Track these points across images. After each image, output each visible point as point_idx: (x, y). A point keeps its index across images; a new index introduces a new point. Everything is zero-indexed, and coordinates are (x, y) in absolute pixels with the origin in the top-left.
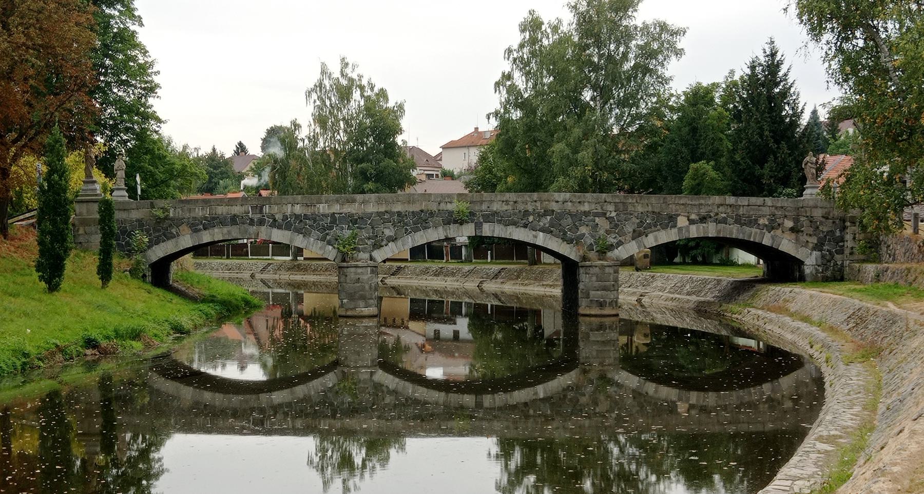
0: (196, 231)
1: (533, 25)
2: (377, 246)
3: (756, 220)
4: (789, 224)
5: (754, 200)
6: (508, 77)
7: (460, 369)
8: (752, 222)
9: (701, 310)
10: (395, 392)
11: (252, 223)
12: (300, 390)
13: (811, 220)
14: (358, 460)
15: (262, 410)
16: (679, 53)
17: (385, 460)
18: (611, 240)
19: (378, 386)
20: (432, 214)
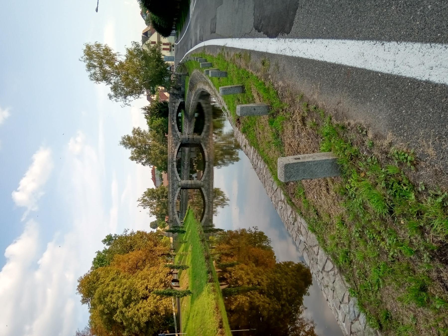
0: (175, 214)
1: (132, 158)
2: (178, 180)
3: (162, 297)
4: (174, 104)
5: (169, 110)
6: (142, 164)
7: (202, 172)
8: (174, 111)
9: (190, 121)
10: (205, 177)
11: (173, 204)
12: (205, 195)
13: (173, 100)
14: (221, 197)
15: (209, 202)
16: (139, 128)
17: (222, 192)
18: (177, 136)
19: (204, 180)
20: (172, 170)
